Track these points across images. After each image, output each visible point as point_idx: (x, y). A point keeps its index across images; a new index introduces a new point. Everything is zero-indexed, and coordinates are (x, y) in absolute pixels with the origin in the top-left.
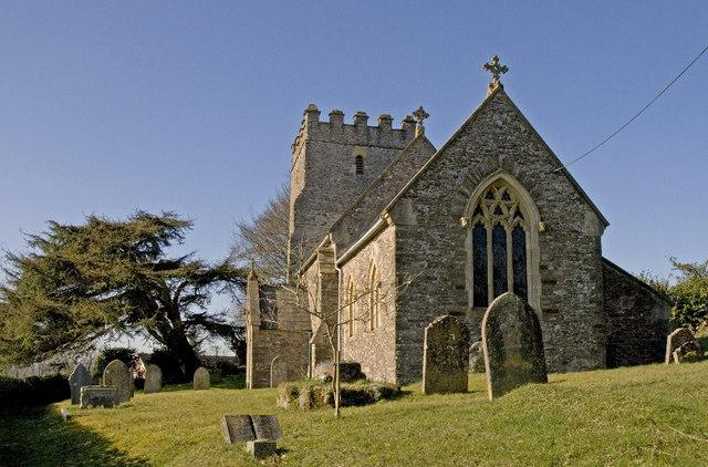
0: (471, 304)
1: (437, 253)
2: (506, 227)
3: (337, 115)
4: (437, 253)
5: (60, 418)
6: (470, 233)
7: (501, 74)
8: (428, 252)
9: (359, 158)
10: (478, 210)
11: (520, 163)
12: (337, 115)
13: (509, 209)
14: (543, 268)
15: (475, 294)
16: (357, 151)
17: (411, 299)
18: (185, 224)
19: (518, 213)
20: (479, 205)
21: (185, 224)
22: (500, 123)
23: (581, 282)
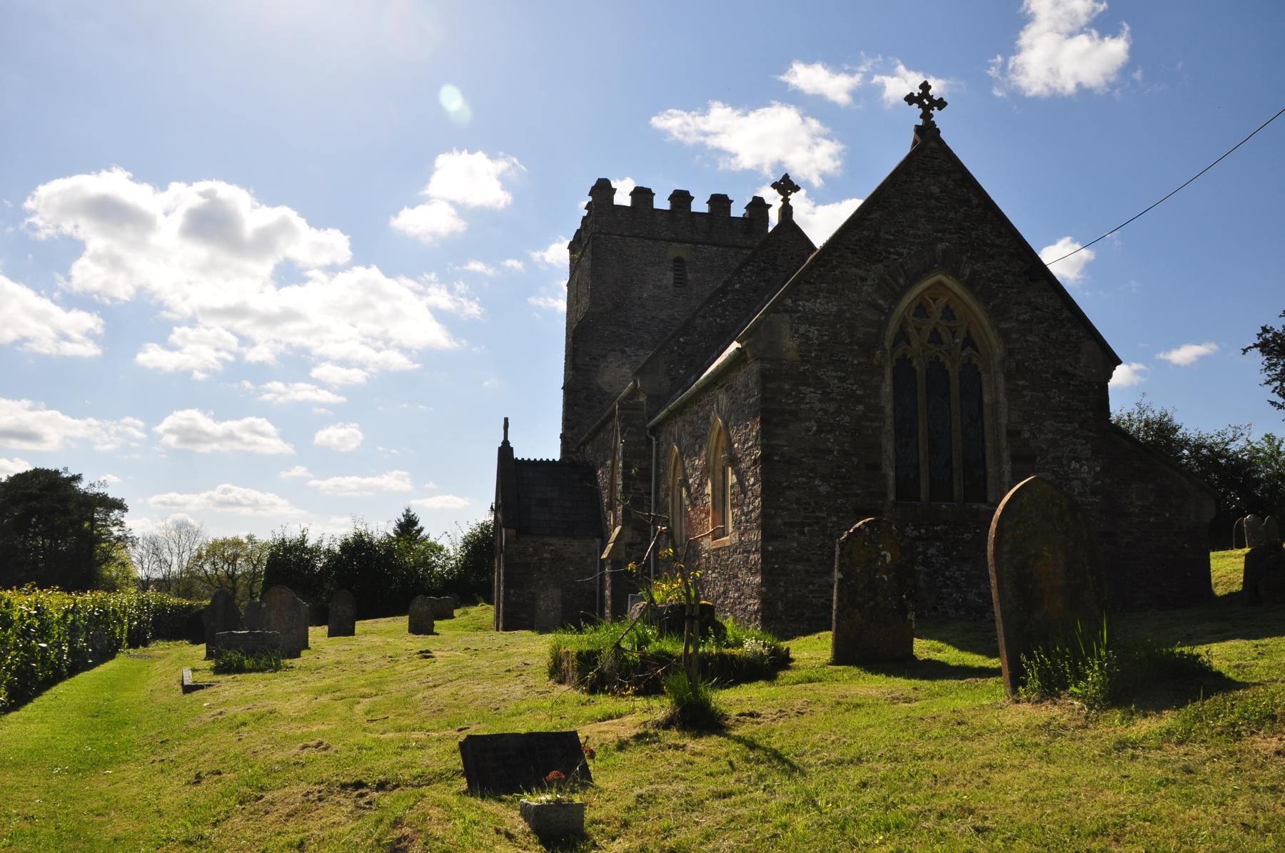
0: (892, 497)
1: (831, 407)
2: (948, 364)
3: (682, 198)
4: (831, 407)
5: (481, 304)
6: (888, 373)
7: (935, 112)
8: (818, 405)
9: (678, 261)
10: (902, 336)
11: (970, 258)
12: (682, 198)
13: (954, 334)
14: (1013, 434)
15: (897, 477)
16: (676, 250)
17: (789, 488)
18: (408, 511)
19: (968, 342)
20: (901, 327)
21: (408, 511)
22: (936, 190)
23: (1078, 459)
